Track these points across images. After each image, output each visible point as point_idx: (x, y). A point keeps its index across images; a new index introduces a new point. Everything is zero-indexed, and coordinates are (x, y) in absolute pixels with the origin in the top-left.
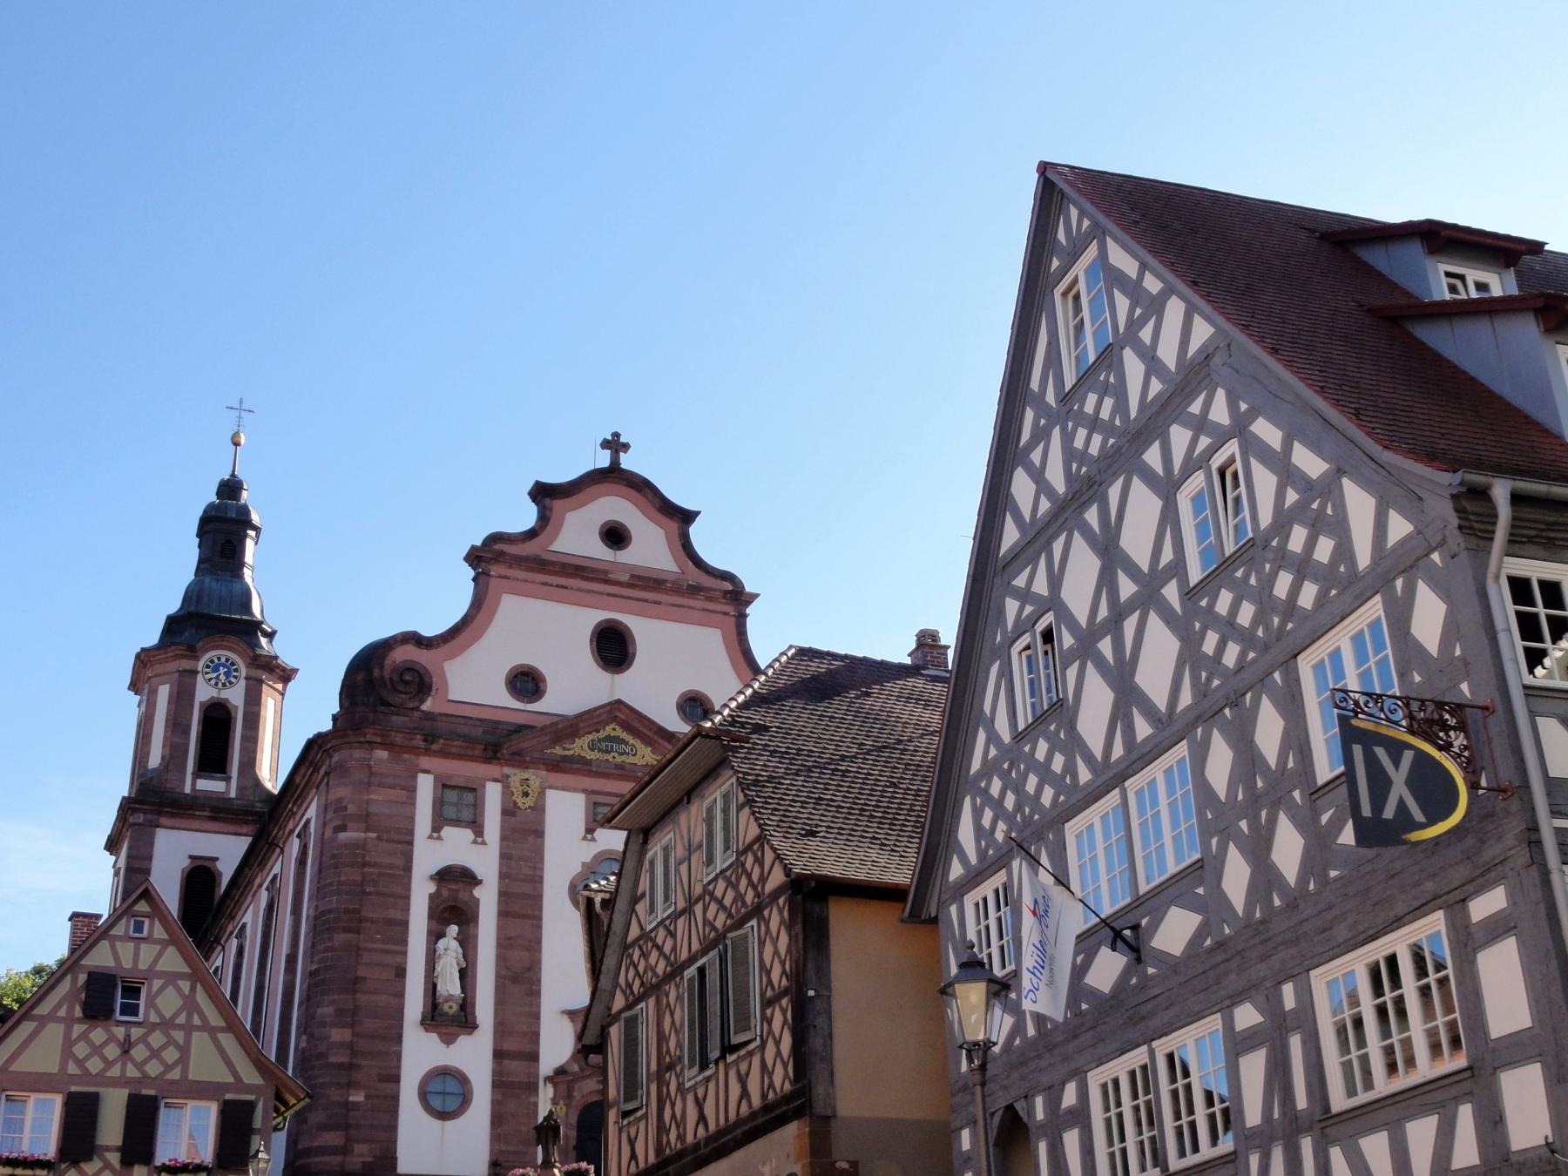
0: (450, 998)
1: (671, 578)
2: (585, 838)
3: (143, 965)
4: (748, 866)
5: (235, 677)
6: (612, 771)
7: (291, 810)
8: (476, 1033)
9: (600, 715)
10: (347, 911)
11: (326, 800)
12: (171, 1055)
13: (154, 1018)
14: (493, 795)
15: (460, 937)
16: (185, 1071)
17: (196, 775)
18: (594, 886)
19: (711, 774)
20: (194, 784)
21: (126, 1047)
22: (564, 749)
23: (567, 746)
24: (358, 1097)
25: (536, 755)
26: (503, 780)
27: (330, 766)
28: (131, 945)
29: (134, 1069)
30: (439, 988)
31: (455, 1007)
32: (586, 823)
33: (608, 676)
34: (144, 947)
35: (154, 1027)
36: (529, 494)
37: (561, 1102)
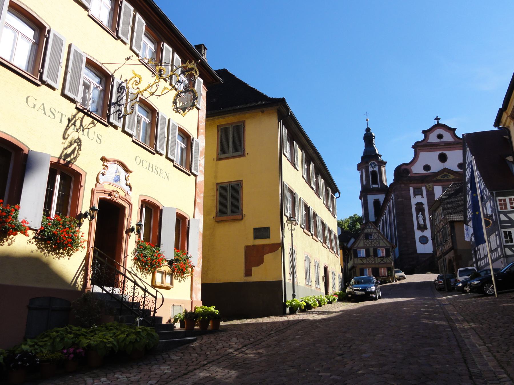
0: (422, 224)
12: (377, 243)
14: (424, 189)
16: (379, 245)
17: (372, 185)
18: (431, 217)
19: (439, 207)
20: (372, 186)
21: (371, 242)
24: (409, 242)
26: (425, 186)
28: (369, 229)
34: (371, 229)
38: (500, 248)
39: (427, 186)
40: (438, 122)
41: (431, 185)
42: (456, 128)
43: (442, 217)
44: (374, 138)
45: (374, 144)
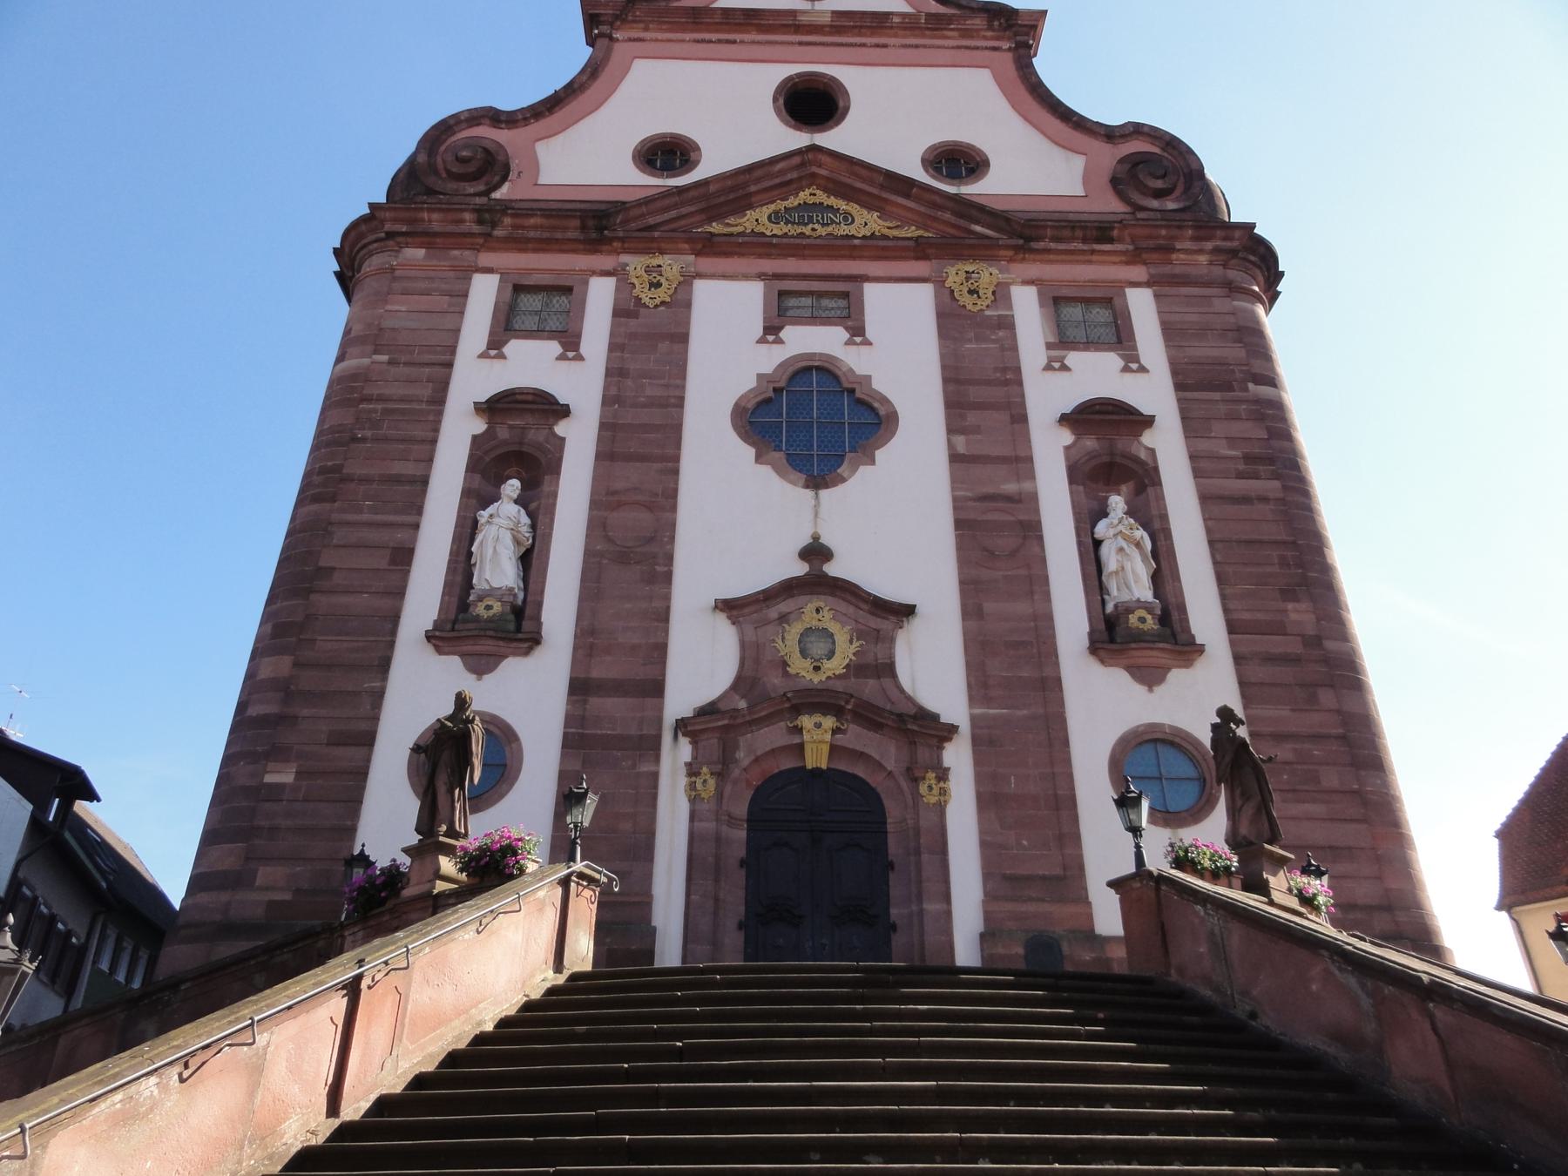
8: (539, 653)
9: (782, 172)
14: (600, 296)
37: (705, 769)
38: (442, 855)
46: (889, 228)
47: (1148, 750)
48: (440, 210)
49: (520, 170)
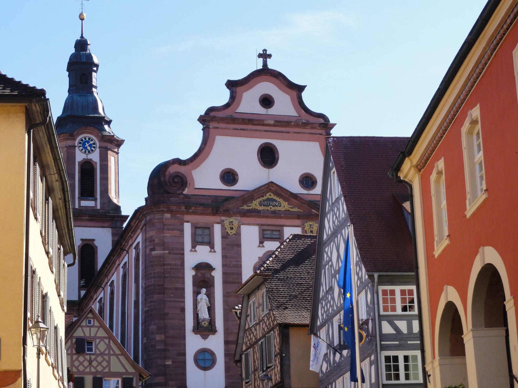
0: (204, 320)
1: (294, 119)
2: (259, 246)
3: (93, 335)
4: (265, 321)
5: (94, 147)
6: (270, 215)
7: (130, 235)
8: (216, 334)
9: (263, 190)
10: (158, 285)
11: (146, 236)
12: (105, 364)
13: (98, 352)
14: (217, 229)
15: (207, 293)
16: (110, 369)
17: (80, 199)
19: (258, 288)
20: (79, 203)
21: (90, 362)
22: (248, 206)
23: (249, 205)
24: (169, 363)
25: (235, 210)
26: (221, 222)
27: (146, 221)
28: (88, 329)
29: (93, 369)
30: (199, 316)
31: (207, 324)
32: (260, 240)
33: (267, 170)
34: (92, 329)
35: (98, 355)
36: (226, 85)
39: (227, 223)
40: (265, 64)
41: (236, 223)
42: (306, 86)
43: (263, 311)
44: (95, 69)
45: (96, 87)
46: (290, 208)
47: (206, 366)
48: (176, 206)
49: (190, 183)
